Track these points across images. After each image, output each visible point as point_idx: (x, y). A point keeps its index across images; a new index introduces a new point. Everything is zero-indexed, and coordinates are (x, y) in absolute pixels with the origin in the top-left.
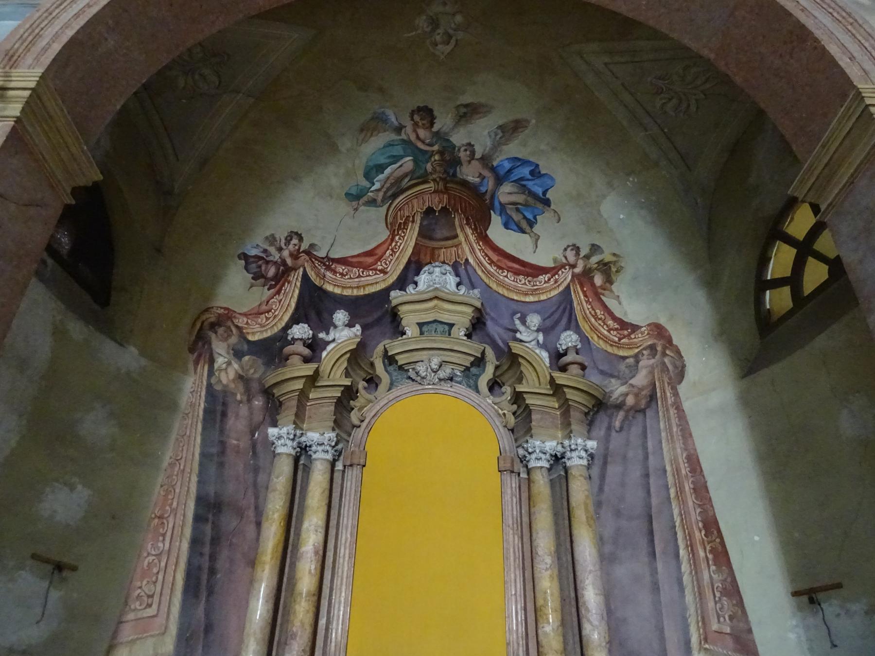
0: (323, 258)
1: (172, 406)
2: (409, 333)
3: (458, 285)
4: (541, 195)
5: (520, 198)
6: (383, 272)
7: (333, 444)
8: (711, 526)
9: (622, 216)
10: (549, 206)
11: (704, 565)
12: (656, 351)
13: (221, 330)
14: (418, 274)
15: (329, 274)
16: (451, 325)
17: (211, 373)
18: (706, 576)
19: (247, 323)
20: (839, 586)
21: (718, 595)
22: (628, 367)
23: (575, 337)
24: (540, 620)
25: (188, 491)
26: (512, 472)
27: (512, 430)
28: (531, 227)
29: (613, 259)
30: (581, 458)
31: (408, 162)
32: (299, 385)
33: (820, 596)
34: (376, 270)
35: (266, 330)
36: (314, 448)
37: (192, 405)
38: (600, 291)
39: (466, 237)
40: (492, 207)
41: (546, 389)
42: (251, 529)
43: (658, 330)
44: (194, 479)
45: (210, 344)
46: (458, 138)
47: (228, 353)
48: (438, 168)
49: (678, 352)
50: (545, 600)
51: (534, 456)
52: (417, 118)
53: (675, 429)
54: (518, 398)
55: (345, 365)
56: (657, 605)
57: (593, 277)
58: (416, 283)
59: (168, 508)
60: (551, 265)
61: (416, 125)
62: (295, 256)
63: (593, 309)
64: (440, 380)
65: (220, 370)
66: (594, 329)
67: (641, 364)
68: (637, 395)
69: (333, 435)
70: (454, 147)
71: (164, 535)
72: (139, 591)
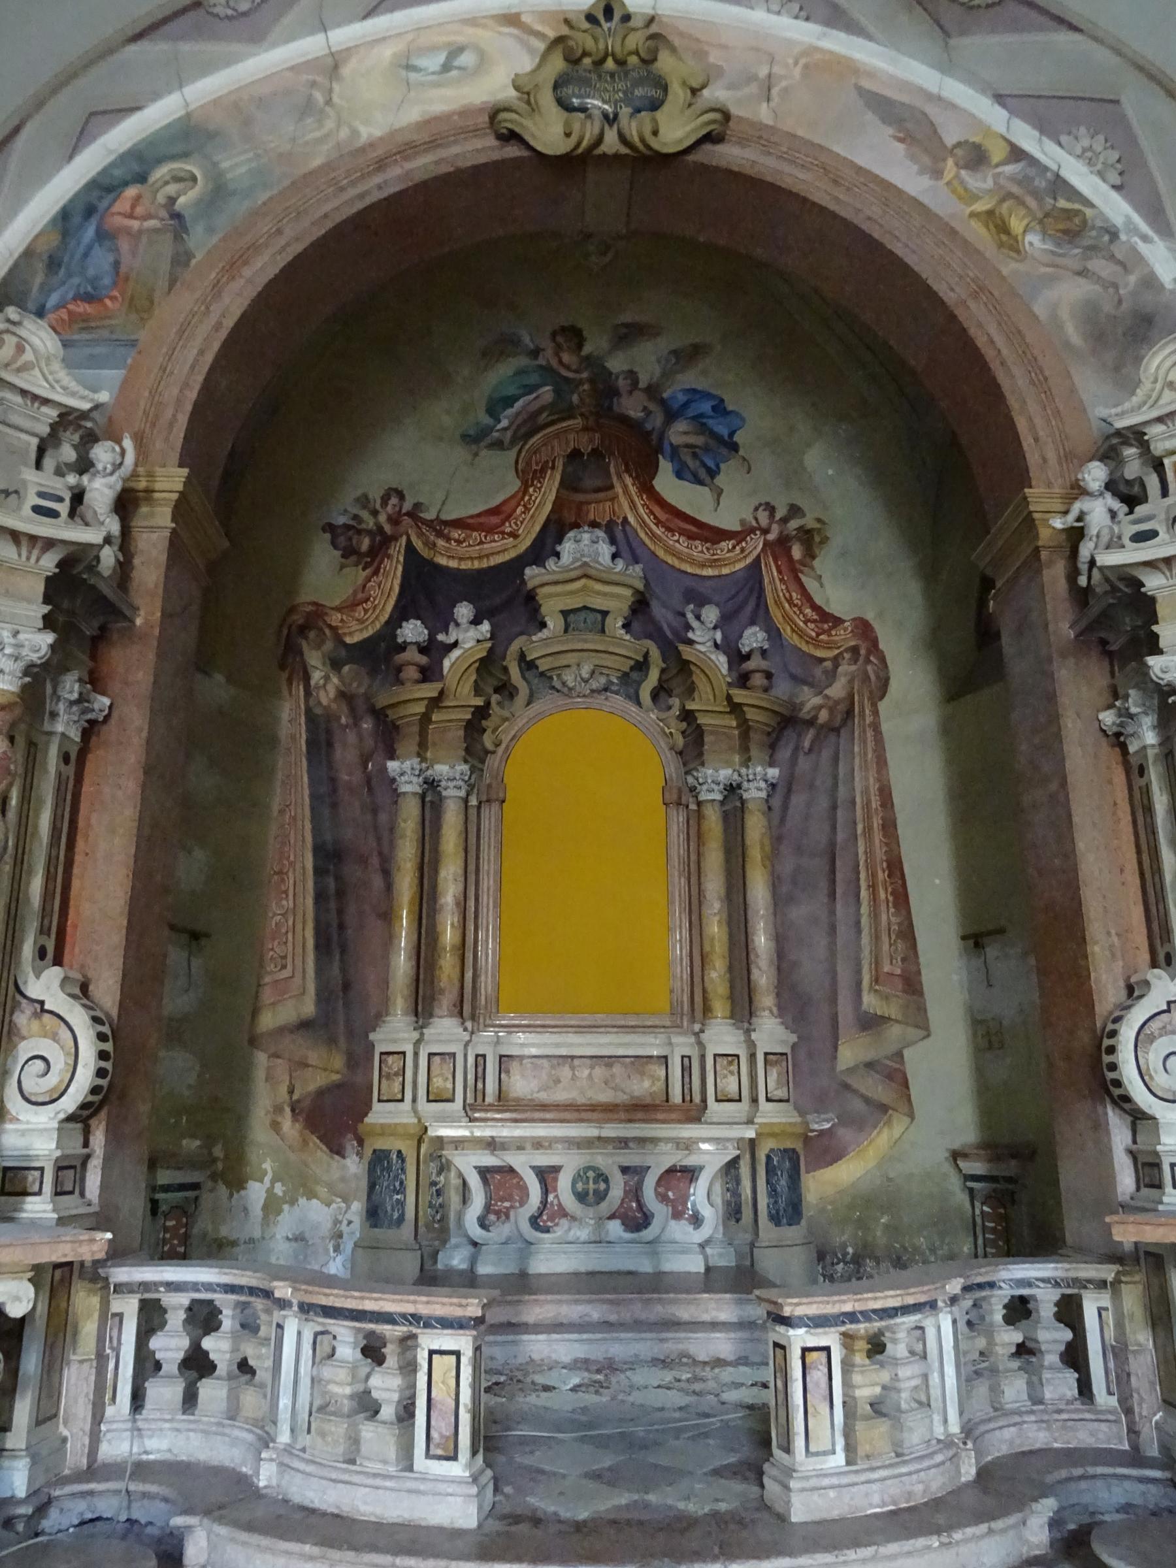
0: (432, 521)
1: (273, 741)
2: (550, 624)
3: (614, 556)
4: (726, 438)
5: (699, 440)
6: (514, 535)
7: (466, 778)
8: (895, 866)
9: (830, 472)
10: (737, 451)
11: (883, 908)
12: (859, 653)
13: (312, 634)
14: (560, 541)
15: (441, 543)
16: (605, 614)
17: (308, 693)
18: (884, 917)
19: (342, 621)
20: (1001, 931)
21: (893, 937)
22: (826, 672)
23: (762, 635)
24: (707, 967)
25: (303, 841)
26: (679, 804)
27: (681, 753)
28: (713, 477)
29: (818, 526)
30: (759, 789)
31: (546, 393)
32: (420, 708)
33: (986, 940)
34: (503, 533)
35: (366, 628)
36: (443, 784)
37: (293, 738)
38: (798, 566)
39: (625, 487)
40: (659, 450)
41: (723, 707)
42: (378, 882)
43: (864, 628)
44: (308, 826)
45: (301, 654)
46: (616, 364)
47: (324, 664)
48: (587, 400)
49: (883, 660)
50: (712, 946)
51: (705, 787)
52: (560, 339)
53: (870, 756)
54: (687, 716)
55: (474, 677)
56: (832, 945)
57: (790, 548)
58: (558, 555)
59: (286, 862)
60: (738, 528)
61: (558, 348)
62: (394, 521)
63: (788, 591)
64: (593, 691)
65: (317, 687)
66: (787, 618)
67: (840, 669)
68: (831, 710)
69: (465, 768)
70: (611, 373)
71: (286, 892)
72: (271, 953)
